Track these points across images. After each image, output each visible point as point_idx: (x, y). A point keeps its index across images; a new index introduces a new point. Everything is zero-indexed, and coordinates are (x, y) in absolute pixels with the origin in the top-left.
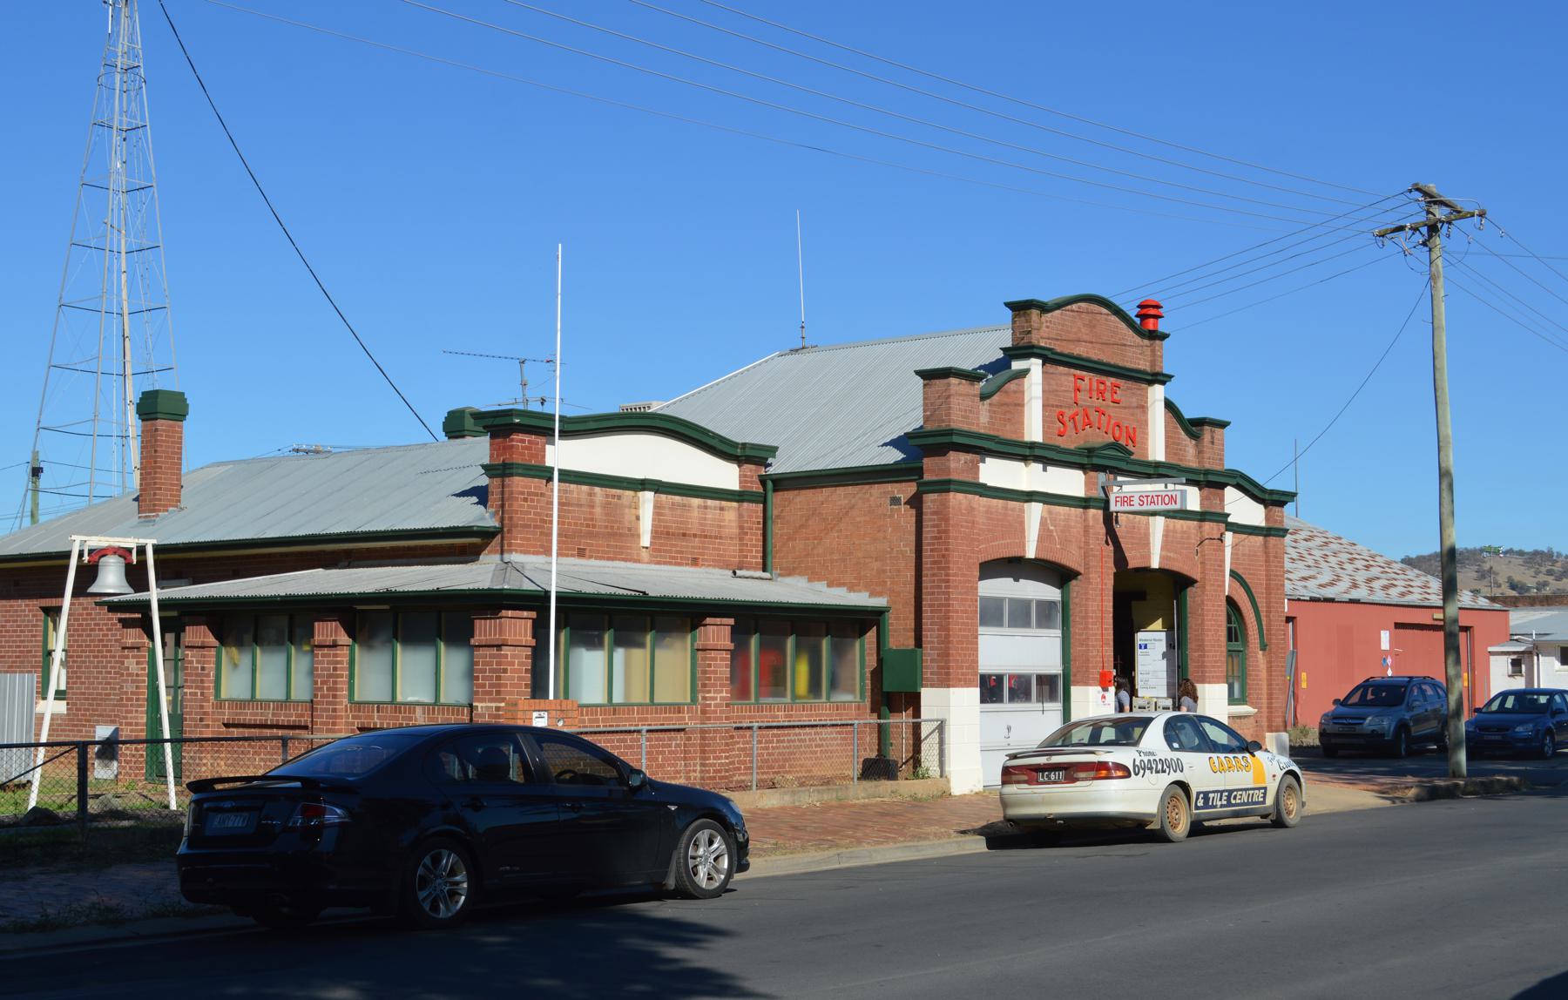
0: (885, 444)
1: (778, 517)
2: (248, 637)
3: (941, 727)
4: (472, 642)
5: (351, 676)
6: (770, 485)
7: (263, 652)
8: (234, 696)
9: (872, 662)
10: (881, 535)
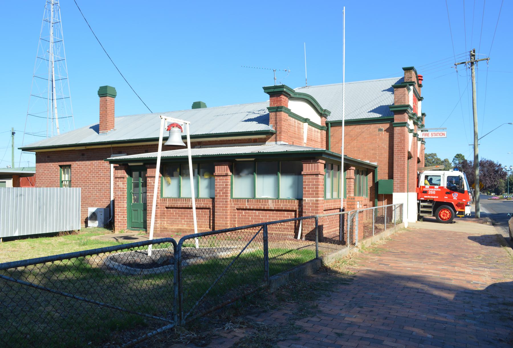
0: (371, 112)
1: (332, 136)
3: (401, 206)
4: (303, 173)
5: (232, 188)
6: (330, 125)
7: (183, 179)
9: (371, 184)
10: (374, 141)
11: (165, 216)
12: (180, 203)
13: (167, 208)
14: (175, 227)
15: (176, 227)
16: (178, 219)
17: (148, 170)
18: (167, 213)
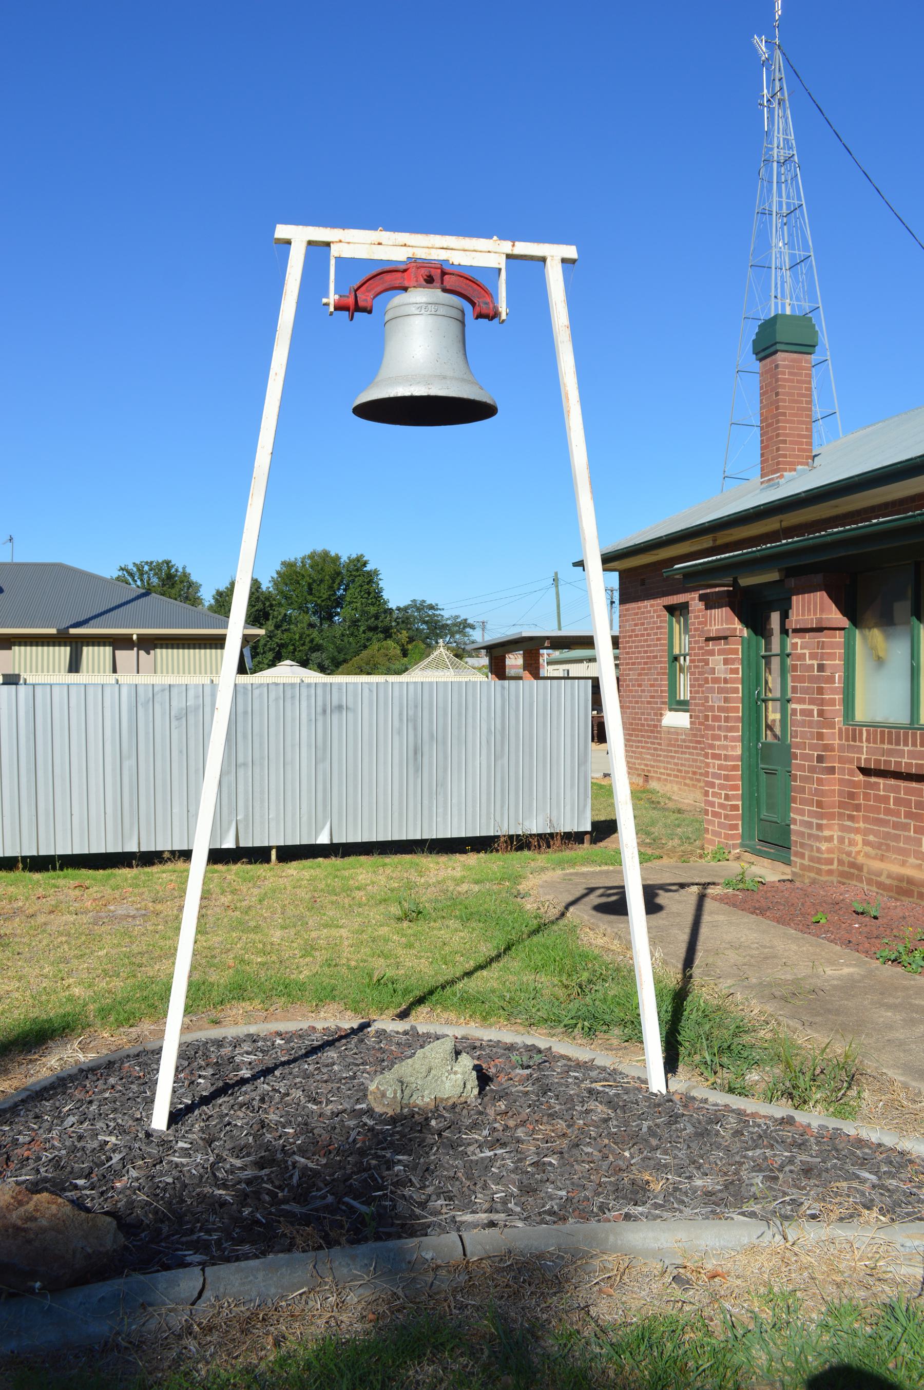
2: (902, 607)
8: (879, 718)
11: (857, 808)
12: (912, 755)
13: (865, 771)
14: (892, 867)
15: (896, 869)
16: (905, 827)
17: (794, 598)
18: (867, 797)
